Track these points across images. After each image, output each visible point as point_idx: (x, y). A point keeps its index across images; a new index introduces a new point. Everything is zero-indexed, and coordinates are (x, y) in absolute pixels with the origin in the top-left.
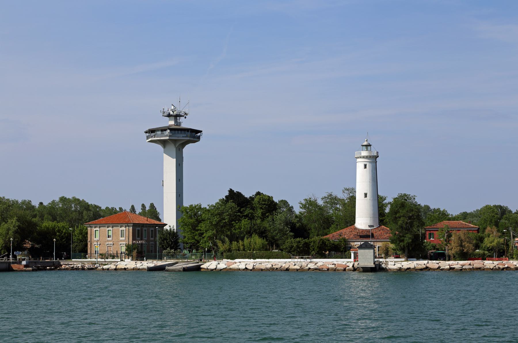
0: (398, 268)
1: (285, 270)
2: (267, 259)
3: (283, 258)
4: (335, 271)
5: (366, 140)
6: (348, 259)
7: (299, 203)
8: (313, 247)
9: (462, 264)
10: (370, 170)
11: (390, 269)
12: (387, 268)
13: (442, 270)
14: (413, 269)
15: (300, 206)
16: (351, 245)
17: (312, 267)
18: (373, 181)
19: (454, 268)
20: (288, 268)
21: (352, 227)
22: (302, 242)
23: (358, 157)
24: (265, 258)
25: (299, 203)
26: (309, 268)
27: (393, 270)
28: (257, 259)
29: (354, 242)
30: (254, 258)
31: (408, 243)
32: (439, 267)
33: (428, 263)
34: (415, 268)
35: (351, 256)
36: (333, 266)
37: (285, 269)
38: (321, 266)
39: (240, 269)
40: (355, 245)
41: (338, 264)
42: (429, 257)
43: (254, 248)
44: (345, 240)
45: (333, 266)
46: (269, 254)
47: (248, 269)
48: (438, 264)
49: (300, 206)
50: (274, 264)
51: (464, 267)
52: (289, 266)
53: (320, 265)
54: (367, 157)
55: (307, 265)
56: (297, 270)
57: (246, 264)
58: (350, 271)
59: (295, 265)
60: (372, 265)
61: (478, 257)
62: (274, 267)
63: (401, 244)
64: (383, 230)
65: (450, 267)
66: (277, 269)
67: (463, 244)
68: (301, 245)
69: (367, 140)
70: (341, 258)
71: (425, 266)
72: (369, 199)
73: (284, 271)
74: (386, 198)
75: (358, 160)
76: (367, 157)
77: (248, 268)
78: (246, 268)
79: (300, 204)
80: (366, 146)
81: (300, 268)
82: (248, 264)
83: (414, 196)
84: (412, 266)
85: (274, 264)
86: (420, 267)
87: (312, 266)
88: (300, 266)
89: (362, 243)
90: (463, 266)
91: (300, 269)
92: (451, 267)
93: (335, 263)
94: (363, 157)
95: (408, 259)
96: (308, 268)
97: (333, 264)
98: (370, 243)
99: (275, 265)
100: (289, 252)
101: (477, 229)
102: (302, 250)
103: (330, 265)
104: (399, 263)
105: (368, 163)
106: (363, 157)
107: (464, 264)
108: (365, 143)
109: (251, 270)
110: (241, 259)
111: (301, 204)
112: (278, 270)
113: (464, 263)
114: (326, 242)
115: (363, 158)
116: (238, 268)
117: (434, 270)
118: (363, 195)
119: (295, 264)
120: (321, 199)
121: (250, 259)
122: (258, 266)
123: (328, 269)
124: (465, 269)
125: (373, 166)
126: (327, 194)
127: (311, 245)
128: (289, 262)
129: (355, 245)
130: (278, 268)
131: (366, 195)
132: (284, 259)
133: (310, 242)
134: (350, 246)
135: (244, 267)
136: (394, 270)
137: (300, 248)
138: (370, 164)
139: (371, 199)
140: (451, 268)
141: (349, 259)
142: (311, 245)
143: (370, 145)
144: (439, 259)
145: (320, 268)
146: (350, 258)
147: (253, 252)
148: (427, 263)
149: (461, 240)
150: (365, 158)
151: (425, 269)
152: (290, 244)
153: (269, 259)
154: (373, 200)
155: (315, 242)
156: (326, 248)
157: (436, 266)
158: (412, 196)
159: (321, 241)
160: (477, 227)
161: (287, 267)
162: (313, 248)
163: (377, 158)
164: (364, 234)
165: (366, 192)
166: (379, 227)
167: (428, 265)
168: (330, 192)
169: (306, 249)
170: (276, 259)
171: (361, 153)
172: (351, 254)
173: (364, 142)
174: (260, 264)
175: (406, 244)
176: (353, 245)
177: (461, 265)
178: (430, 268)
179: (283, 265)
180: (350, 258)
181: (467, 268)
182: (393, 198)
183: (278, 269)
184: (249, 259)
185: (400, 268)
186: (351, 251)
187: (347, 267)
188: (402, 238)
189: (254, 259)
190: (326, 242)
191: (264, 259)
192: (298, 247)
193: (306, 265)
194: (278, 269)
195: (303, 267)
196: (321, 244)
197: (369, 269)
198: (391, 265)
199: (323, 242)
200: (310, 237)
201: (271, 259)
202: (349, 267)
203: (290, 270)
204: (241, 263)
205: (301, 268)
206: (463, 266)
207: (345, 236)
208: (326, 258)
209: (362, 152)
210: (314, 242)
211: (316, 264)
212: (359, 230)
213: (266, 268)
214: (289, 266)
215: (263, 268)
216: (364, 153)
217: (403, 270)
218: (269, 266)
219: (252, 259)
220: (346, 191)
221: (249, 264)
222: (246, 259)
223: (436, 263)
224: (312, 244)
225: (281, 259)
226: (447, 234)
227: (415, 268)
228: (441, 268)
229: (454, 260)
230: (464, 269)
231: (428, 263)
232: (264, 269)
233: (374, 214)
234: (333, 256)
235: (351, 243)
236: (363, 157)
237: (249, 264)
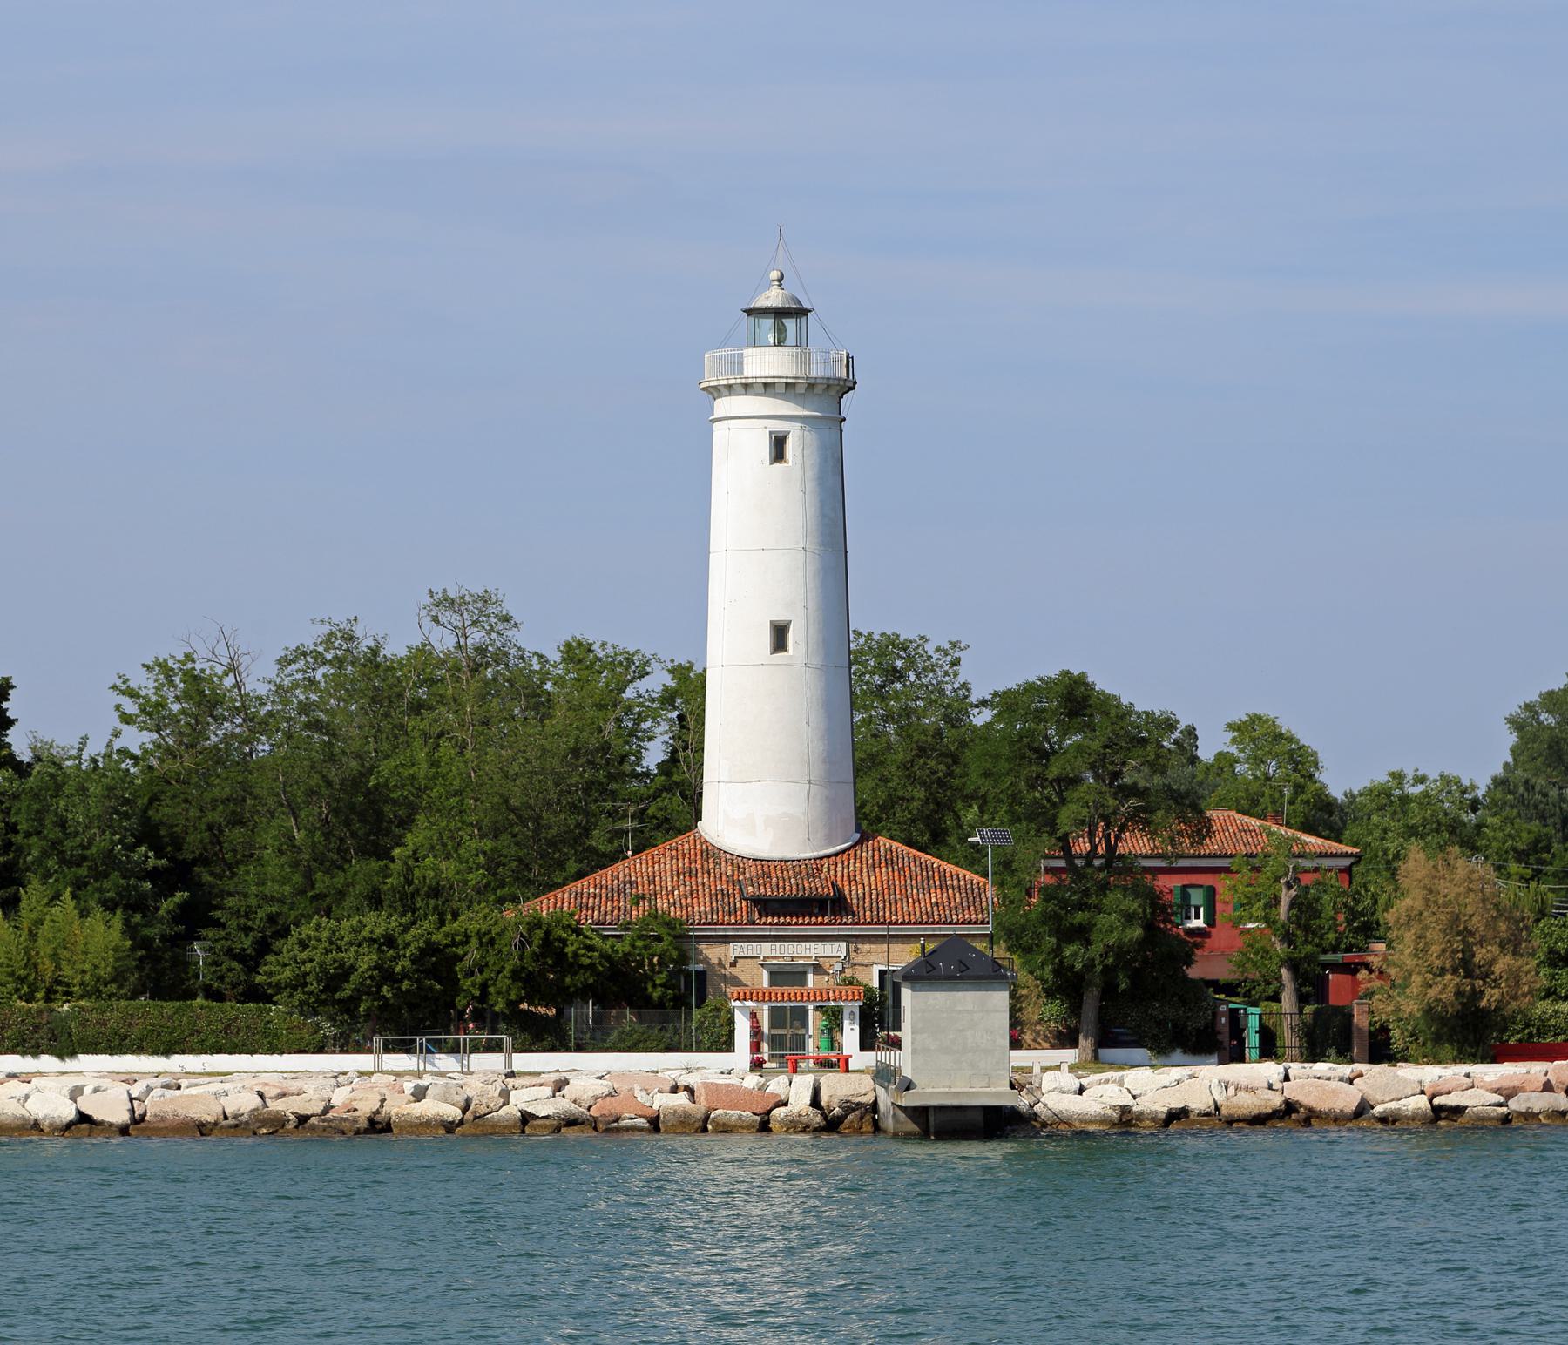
0: (1109, 1112)
1: (366, 1131)
2: (155, 1052)
3: (272, 1050)
4: (705, 1130)
5: (775, 275)
6: (709, 1050)
7: (114, 687)
8: (481, 972)
9: (1504, 1084)
10: (809, 474)
11: (1060, 1120)
12: (1038, 1108)
13: (1383, 1119)
14: (1208, 1114)
15: (118, 708)
16: (706, 960)
17: (542, 1110)
18: (823, 544)
19: (1458, 1110)
20: (378, 1112)
21: (683, 843)
22: (408, 945)
23: (729, 387)
24: (138, 1049)
25: (114, 687)
26: (526, 1118)
27: (1081, 1121)
28: (80, 1056)
29: (727, 939)
30: (66, 1048)
31: (1119, 951)
32: (1363, 1109)
33: (1287, 1078)
34: (1217, 1108)
35: (731, 1033)
36: (681, 1099)
37: (363, 1124)
38: (596, 1098)
39: (36, 1126)
40: (733, 964)
41: (711, 1088)
42: (572, 1045)
43: (57, 982)
44: (680, 936)
45: (681, 1099)
46: (171, 1018)
47: (101, 1123)
48: (1351, 1081)
49: (118, 708)
50: (270, 1092)
51: (1515, 1105)
52: (383, 1101)
53: (591, 1094)
54: (788, 389)
55: (505, 1094)
56: (450, 1127)
57: (75, 1093)
58: (803, 1131)
59: (420, 1094)
60: (998, 1094)
61: (1520, 1041)
62: (275, 1106)
63: (1075, 954)
64: (890, 862)
65: (1431, 1101)
66: (303, 1119)
67: (1480, 955)
68: (405, 963)
69: (780, 280)
70: (669, 1049)
71: (1276, 1101)
72: (801, 660)
73: (357, 1132)
74: (647, 663)
75: (724, 406)
76: (788, 389)
77: (97, 1116)
78: (83, 1118)
79: (123, 693)
80: (780, 313)
81: (464, 1112)
82: (87, 1090)
83: (954, 645)
84: (1198, 1101)
85: (275, 1092)
86: (1248, 1103)
87: (532, 1099)
88: (460, 1099)
89: (930, 947)
90: (1509, 1093)
91: (461, 1122)
92: (1436, 1101)
93: (693, 1080)
94: (768, 388)
95: (1106, 1053)
96: (511, 1111)
97: (675, 1089)
98: (981, 946)
99: (283, 1095)
100: (310, 1008)
101: (1346, 862)
102: (408, 991)
103: (659, 1091)
104: (1107, 1081)
105: (798, 425)
106: (768, 388)
107: (1516, 1083)
108: (773, 298)
109: (124, 1130)
110: (313, 1053)
111: (132, 694)
112: (313, 1128)
113: (1510, 1077)
114: (564, 942)
115: (765, 394)
116: (23, 1117)
117: (1338, 1119)
118: (766, 638)
119: (417, 1087)
120: (279, 662)
121: (36, 1051)
122: (158, 1104)
123: (655, 1123)
124: (1529, 1116)
125: (823, 447)
126: (326, 629)
127: (467, 963)
128: (361, 1074)
129: (733, 964)
130: (307, 1118)
131: (780, 636)
132: (276, 1056)
133: (454, 944)
134: (701, 967)
135: (67, 1112)
136: (1091, 1122)
137: (401, 981)
138: (811, 437)
139: (816, 661)
140: (1438, 1111)
141: (719, 1050)
142: (467, 963)
143: (800, 312)
144: (1332, 1051)
145: (593, 1112)
146: (727, 1045)
147: (52, 1010)
148: (1282, 1076)
149: (1468, 932)
150: (775, 396)
151: (1281, 1118)
152: (327, 952)
153: (167, 1052)
154: (827, 668)
155: (492, 942)
156: (568, 980)
157: (1347, 1100)
158: (938, 650)
159: (539, 933)
160: (1350, 850)
161: (366, 1107)
162: (479, 978)
163: (845, 395)
164: (790, 887)
165: (781, 617)
166: (859, 842)
167: (1294, 1091)
168: (340, 618)
169: (438, 987)
170: (219, 1052)
171: (739, 363)
172: (731, 1022)
173: (766, 286)
174: (167, 1086)
175: (1104, 956)
176: (715, 961)
177: (1497, 1091)
178: (1311, 1110)
179: (339, 1098)
180: (727, 1045)
181: (1536, 1111)
182: (670, 665)
183: (314, 1120)
184: (24, 1054)
185: (1125, 1110)
186: (734, 1004)
187: (777, 1105)
188: (1080, 917)
189: (61, 1056)
190: (564, 942)
191: (133, 1052)
192: (385, 975)
193: (494, 1091)
194: (314, 1120)
195: (483, 1109)
196: (534, 953)
197: (979, 1117)
198: (1062, 1092)
199: (547, 941)
200: (860, 946)
201: (183, 1052)
202: (785, 1104)
203: (401, 1128)
204: (35, 1081)
205: (469, 1115)
206: (1509, 1097)
207: (662, 904)
208: (568, 1050)
209: (748, 352)
210: (488, 941)
211: (560, 1086)
212: (737, 861)
213: (226, 1118)
214: (383, 1101)
215: (206, 1112)
216: (765, 362)
217: (1148, 1123)
218: (242, 1102)
219: (45, 1058)
220: (447, 616)
221: (96, 1090)
222: (125, 1053)
223: (1341, 1080)
224: (473, 953)
225: (252, 1052)
226: (1293, 893)
227: (1217, 1108)
228: (1378, 1109)
229: (1474, 1055)
230: (1520, 1114)
231: (1287, 1078)
232: (216, 1124)
233: (829, 760)
234: (614, 1036)
235: (703, 946)
236: (765, 385)
237: (96, 1090)
